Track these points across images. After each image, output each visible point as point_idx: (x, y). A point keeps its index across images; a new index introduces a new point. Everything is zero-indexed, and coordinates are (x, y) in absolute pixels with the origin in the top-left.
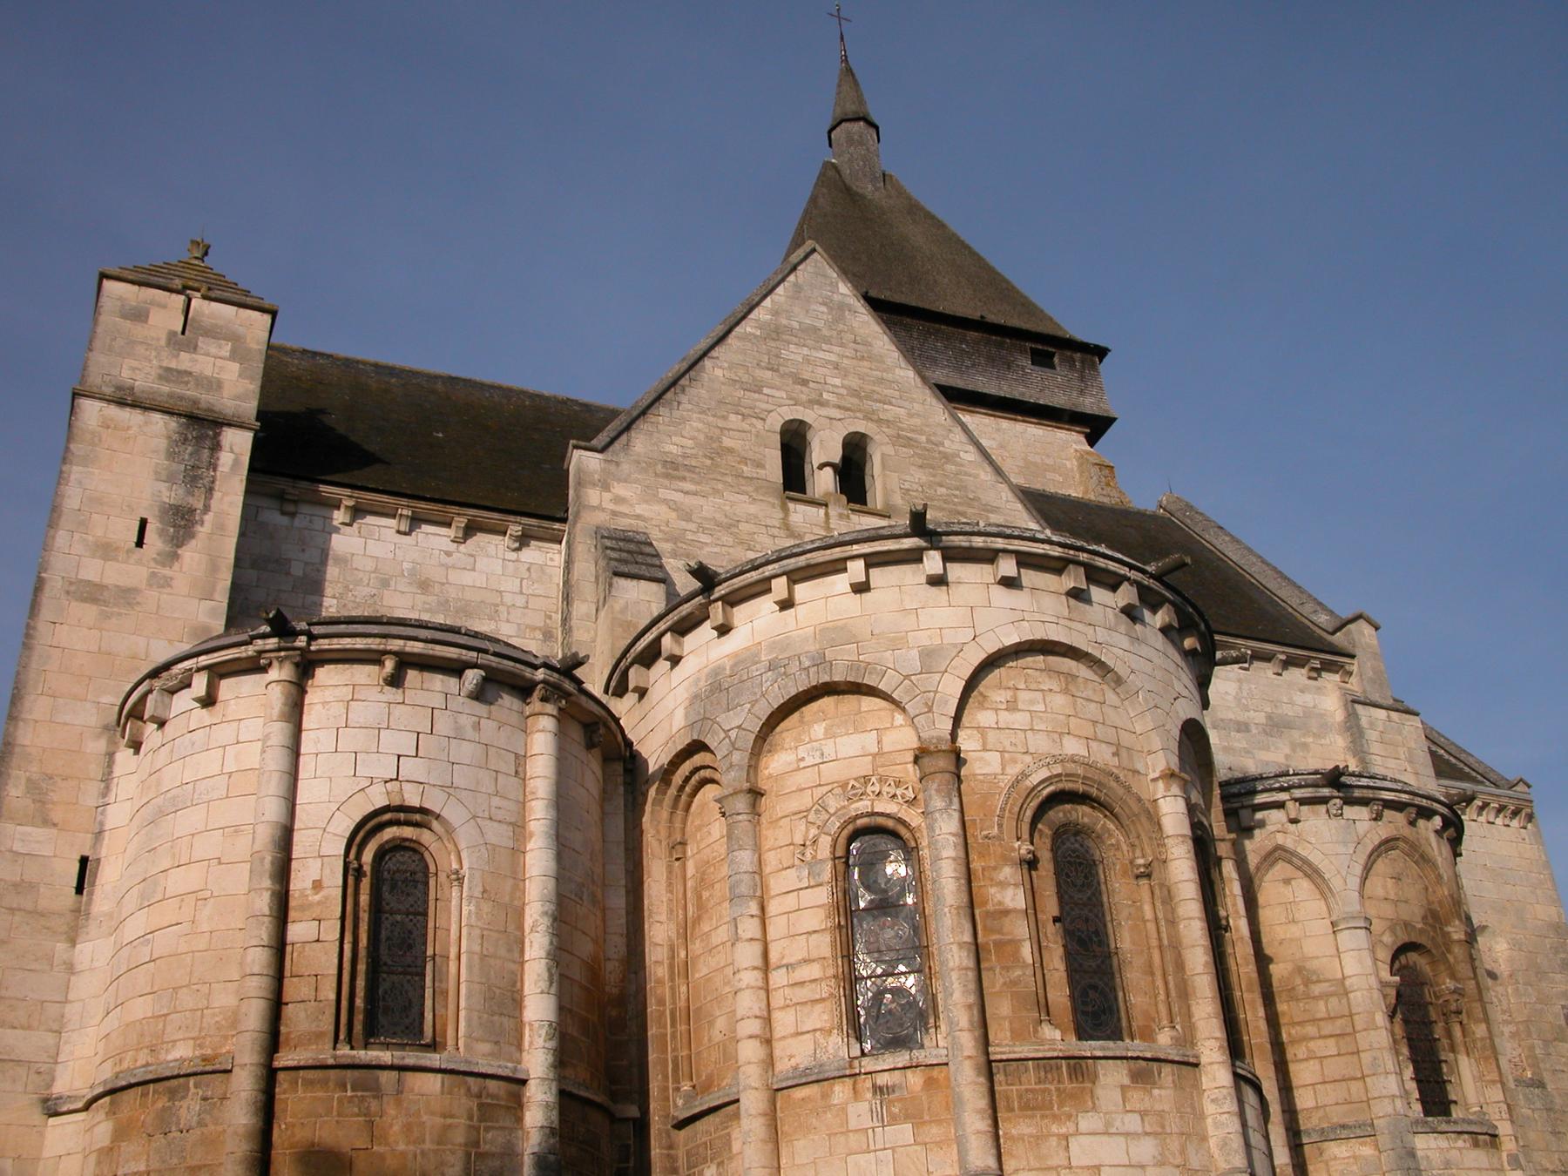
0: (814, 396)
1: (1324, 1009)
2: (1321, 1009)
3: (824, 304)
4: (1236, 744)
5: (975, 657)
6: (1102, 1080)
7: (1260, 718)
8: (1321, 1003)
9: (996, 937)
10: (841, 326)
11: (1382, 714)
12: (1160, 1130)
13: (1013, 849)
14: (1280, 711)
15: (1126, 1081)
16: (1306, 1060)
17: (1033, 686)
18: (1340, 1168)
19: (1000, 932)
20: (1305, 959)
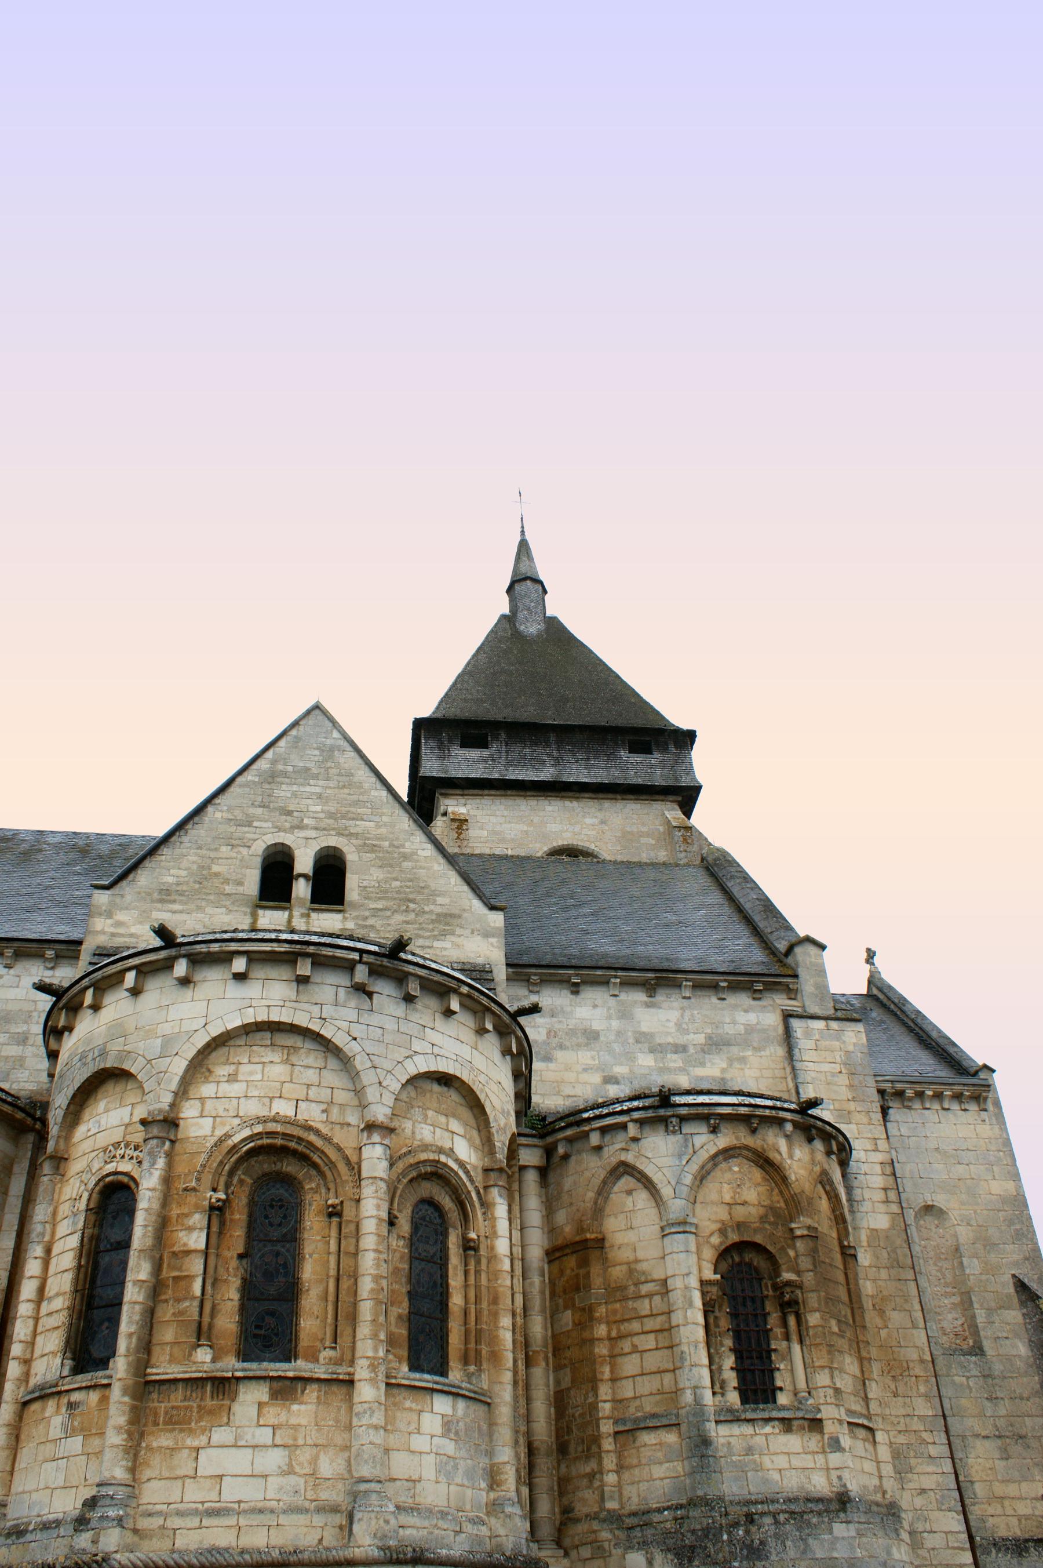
0: (296, 822)
1: (648, 1307)
2: (644, 1307)
3: (318, 749)
4: (672, 1065)
5: (201, 1040)
6: (241, 1397)
7: (701, 1039)
8: (647, 1301)
9: (176, 1274)
10: (329, 764)
11: (820, 1024)
12: (291, 1442)
13: (205, 1199)
14: (720, 1031)
15: (265, 1398)
16: (630, 1353)
17: (256, 1060)
18: (649, 1454)
19: (180, 1269)
20: (637, 1261)
